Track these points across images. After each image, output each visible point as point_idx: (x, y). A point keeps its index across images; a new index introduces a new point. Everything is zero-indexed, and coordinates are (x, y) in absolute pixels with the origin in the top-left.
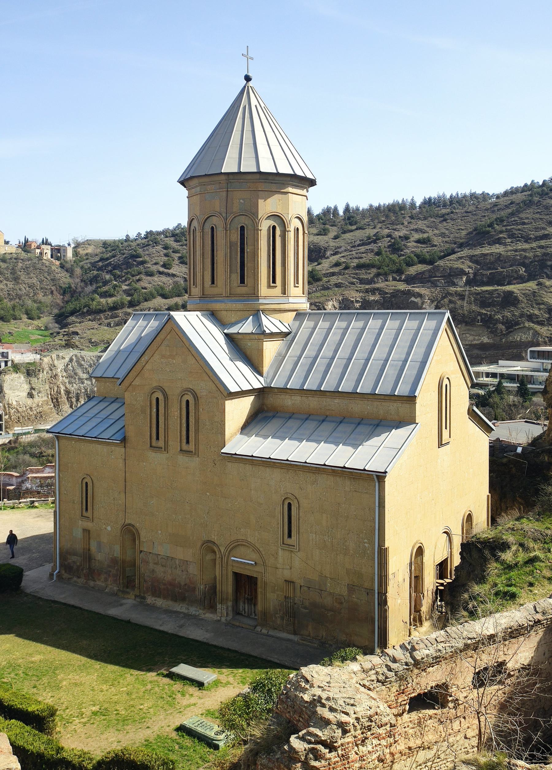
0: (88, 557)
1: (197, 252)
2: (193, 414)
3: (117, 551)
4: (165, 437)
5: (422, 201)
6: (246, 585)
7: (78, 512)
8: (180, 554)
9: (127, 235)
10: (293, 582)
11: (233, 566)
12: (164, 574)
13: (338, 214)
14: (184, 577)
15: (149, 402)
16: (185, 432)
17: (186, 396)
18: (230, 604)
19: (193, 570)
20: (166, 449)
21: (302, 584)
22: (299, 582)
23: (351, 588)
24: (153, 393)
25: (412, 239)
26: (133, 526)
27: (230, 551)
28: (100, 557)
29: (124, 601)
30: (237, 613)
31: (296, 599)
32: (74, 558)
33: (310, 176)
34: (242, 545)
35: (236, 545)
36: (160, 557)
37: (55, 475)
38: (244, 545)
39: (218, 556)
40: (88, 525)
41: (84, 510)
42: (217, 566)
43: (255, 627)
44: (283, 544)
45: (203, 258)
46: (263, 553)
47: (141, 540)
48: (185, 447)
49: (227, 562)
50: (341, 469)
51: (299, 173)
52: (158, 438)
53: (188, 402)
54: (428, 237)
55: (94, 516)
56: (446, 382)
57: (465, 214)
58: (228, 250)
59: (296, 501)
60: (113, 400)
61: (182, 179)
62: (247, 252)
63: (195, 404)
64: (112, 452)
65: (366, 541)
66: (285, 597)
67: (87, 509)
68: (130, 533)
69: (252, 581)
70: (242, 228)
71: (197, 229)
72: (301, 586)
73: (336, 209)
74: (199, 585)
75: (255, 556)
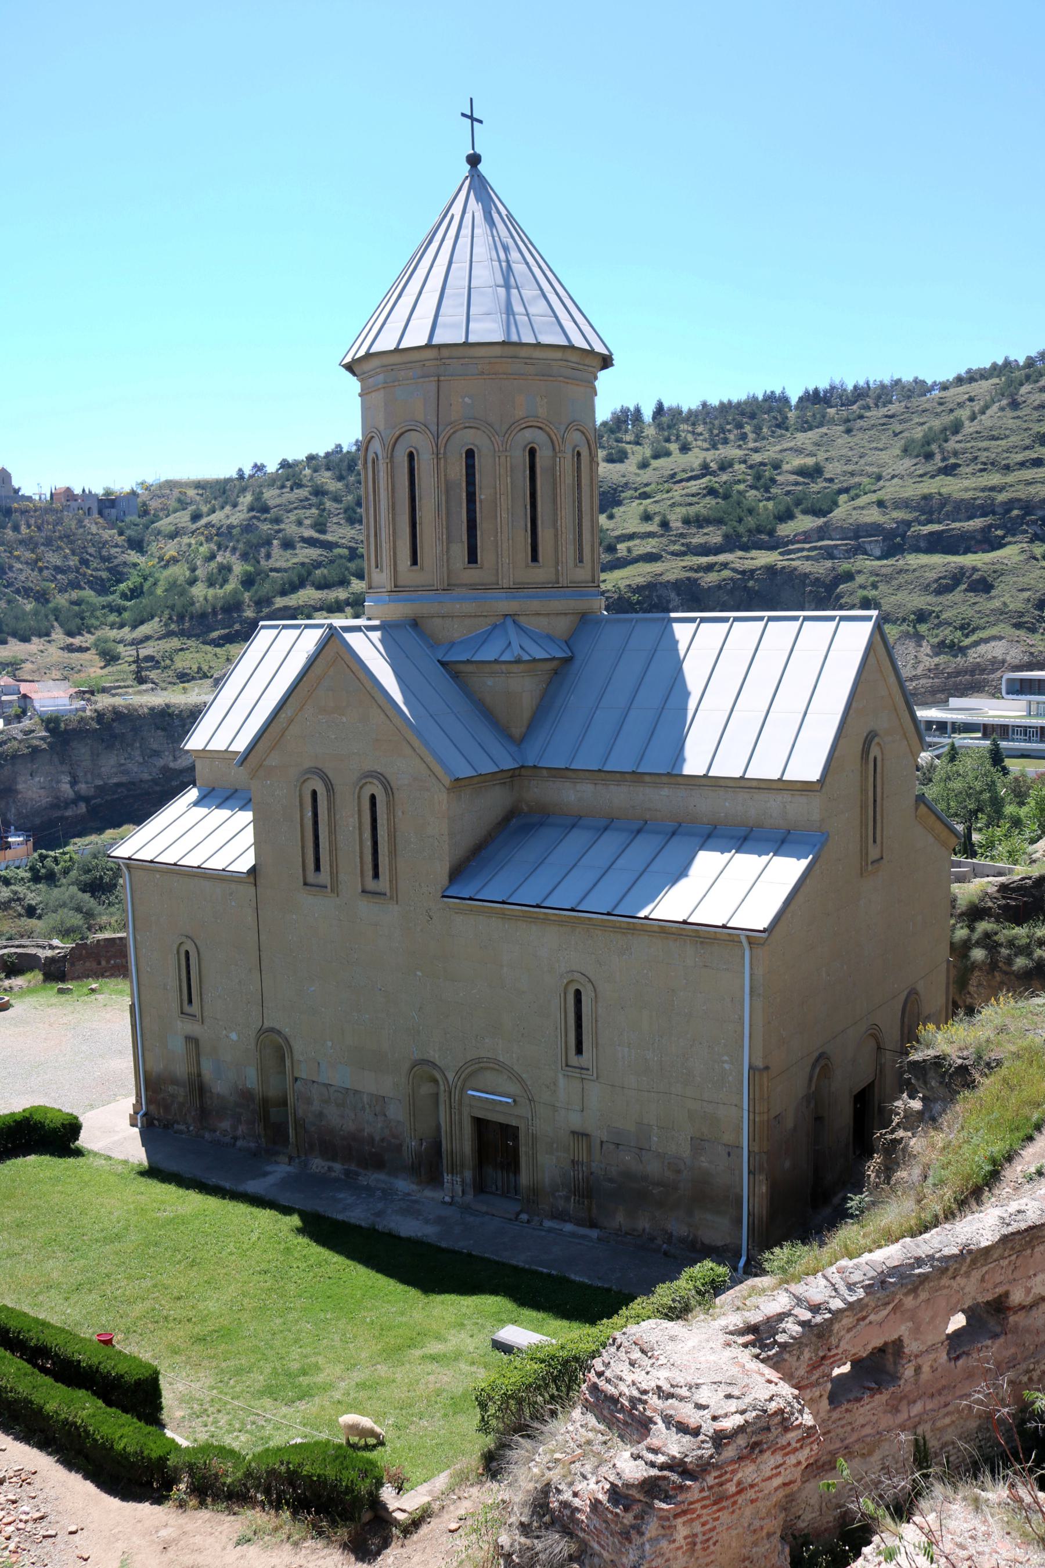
0: (198, 1088)
1: (382, 503)
2: (385, 822)
3: (251, 1079)
4: (331, 866)
5: (801, 394)
6: (497, 1144)
7: (175, 1006)
8: (370, 1084)
9: (240, 470)
10: (587, 1135)
11: (471, 1106)
12: (340, 1120)
13: (642, 421)
14: (379, 1125)
15: (298, 800)
16: (370, 857)
17: (368, 786)
18: (468, 1175)
19: (397, 1112)
20: (335, 888)
21: (605, 1139)
22: (599, 1134)
23: (698, 1144)
24: (305, 781)
25: (786, 467)
26: (279, 1033)
27: (465, 1080)
28: (220, 1087)
29: (269, 1168)
30: (480, 1187)
31: (594, 1165)
32: (171, 1089)
33: (599, 348)
34: (487, 1069)
35: (475, 1069)
36: (332, 1090)
37: (128, 934)
38: (493, 1069)
39: (442, 1088)
40: (193, 1028)
41: (186, 1002)
42: (442, 1108)
43: (518, 1214)
44: (567, 1066)
45: (394, 515)
46: (529, 1083)
47: (295, 1058)
48: (371, 884)
49: (460, 1104)
50: (559, 355)
51: (579, 342)
52: (317, 868)
53: (373, 798)
54: (817, 464)
55: (205, 1014)
56: (875, 751)
57: (884, 420)
58: (444, 498)
59: (589, 986)
60: (227, 794)
61: (348, 359)
62: (481, 501)
63: (388, 803)
64: (231, 894)
65: (726, 1058)
66: (573, 1161)
67: (190, 1001)
68: (274, 1048)
69: (509, 1132)
70: (470, 454)
71: (380, 457)
72: (602, 1142)
73: (638, 410)
74: (408, 1139)
75: (513, 1088)
